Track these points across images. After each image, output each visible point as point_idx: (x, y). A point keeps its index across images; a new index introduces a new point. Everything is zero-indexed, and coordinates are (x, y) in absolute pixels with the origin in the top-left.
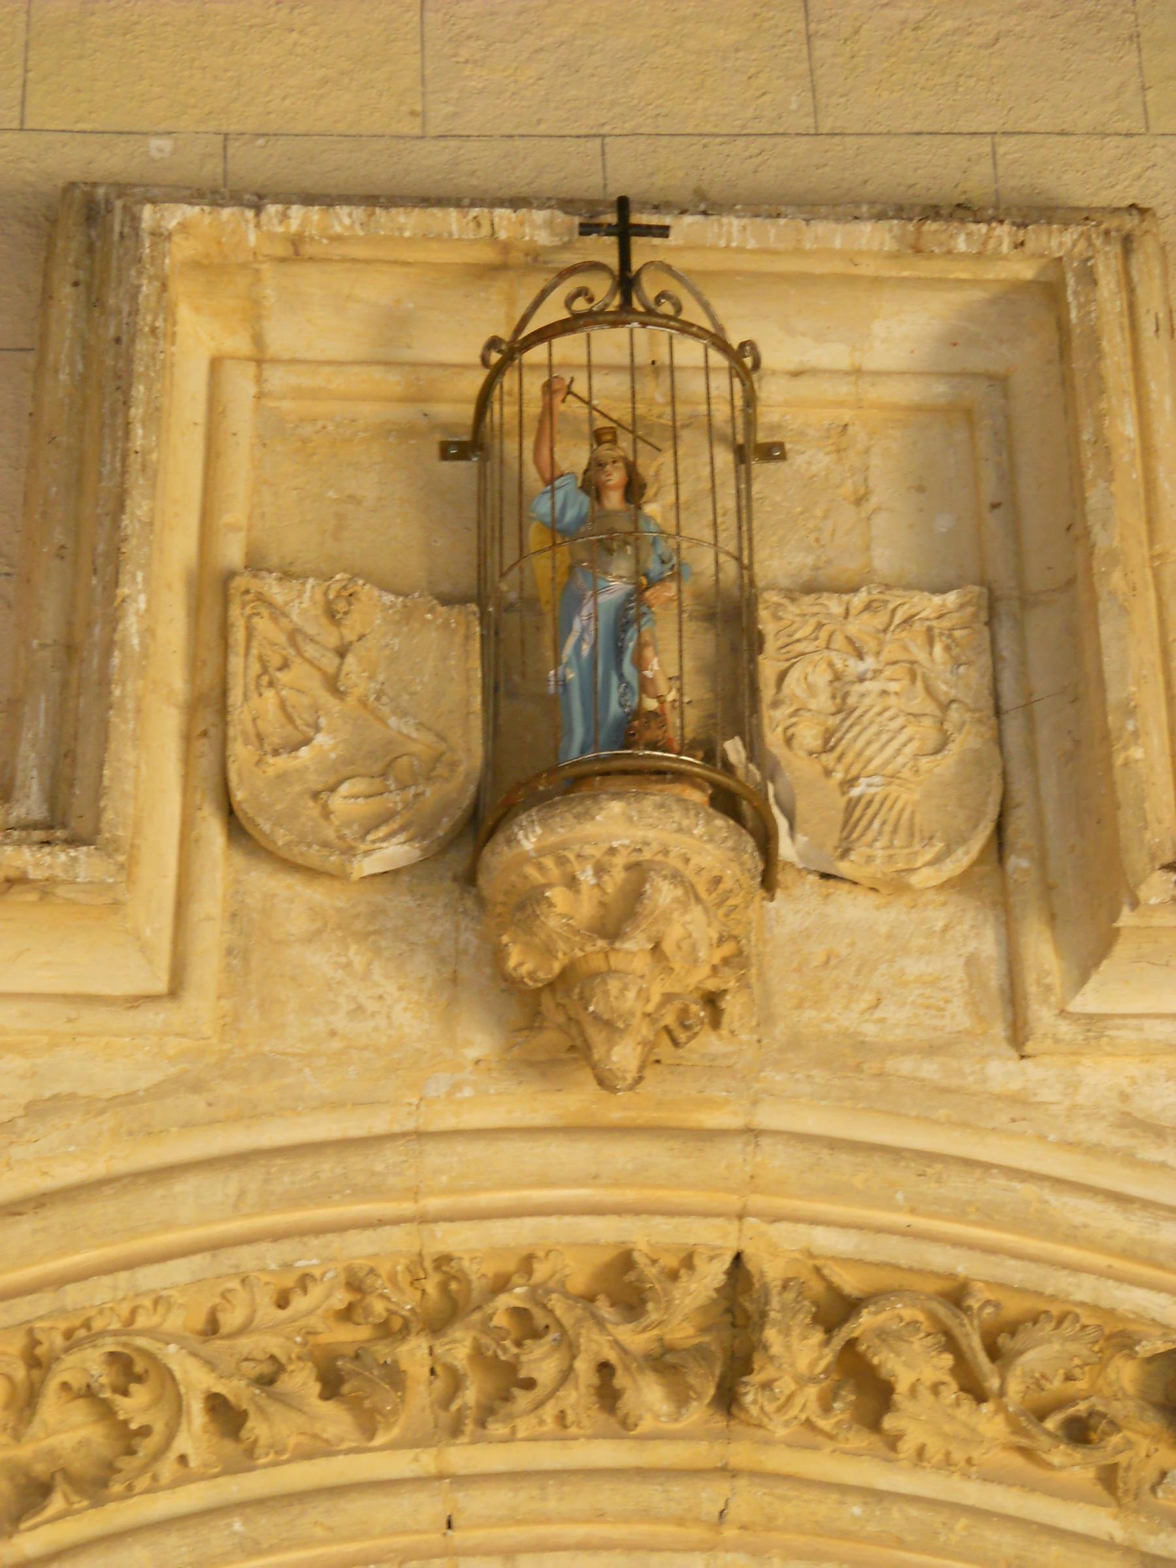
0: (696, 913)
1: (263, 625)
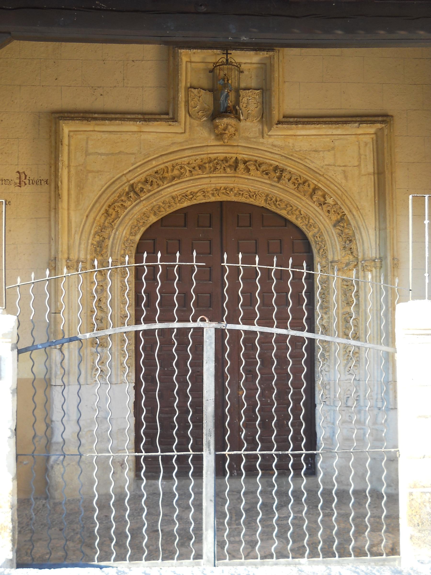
0: (233, 128)
1: (192, 94)
